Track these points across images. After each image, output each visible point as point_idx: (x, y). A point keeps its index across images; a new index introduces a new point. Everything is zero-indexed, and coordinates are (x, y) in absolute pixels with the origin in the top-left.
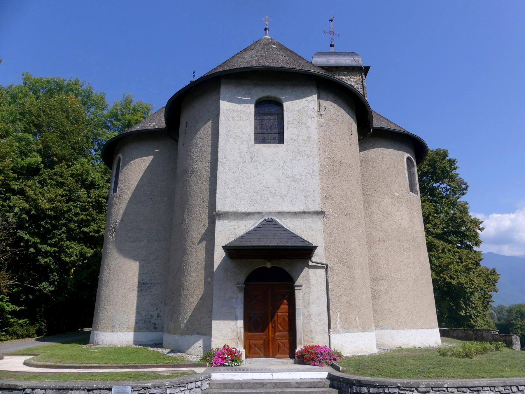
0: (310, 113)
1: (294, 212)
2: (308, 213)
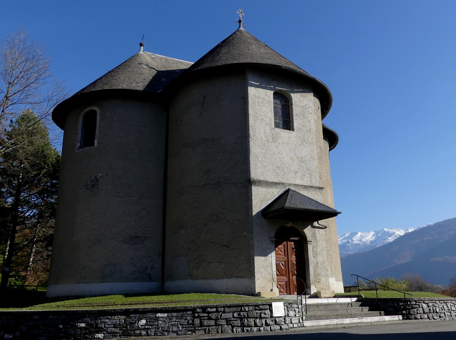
0: (310, 110)
1: (305, 186)
2: (314, 187)
